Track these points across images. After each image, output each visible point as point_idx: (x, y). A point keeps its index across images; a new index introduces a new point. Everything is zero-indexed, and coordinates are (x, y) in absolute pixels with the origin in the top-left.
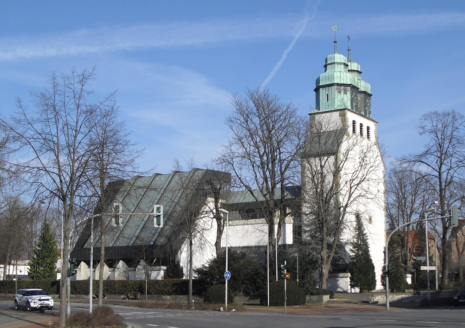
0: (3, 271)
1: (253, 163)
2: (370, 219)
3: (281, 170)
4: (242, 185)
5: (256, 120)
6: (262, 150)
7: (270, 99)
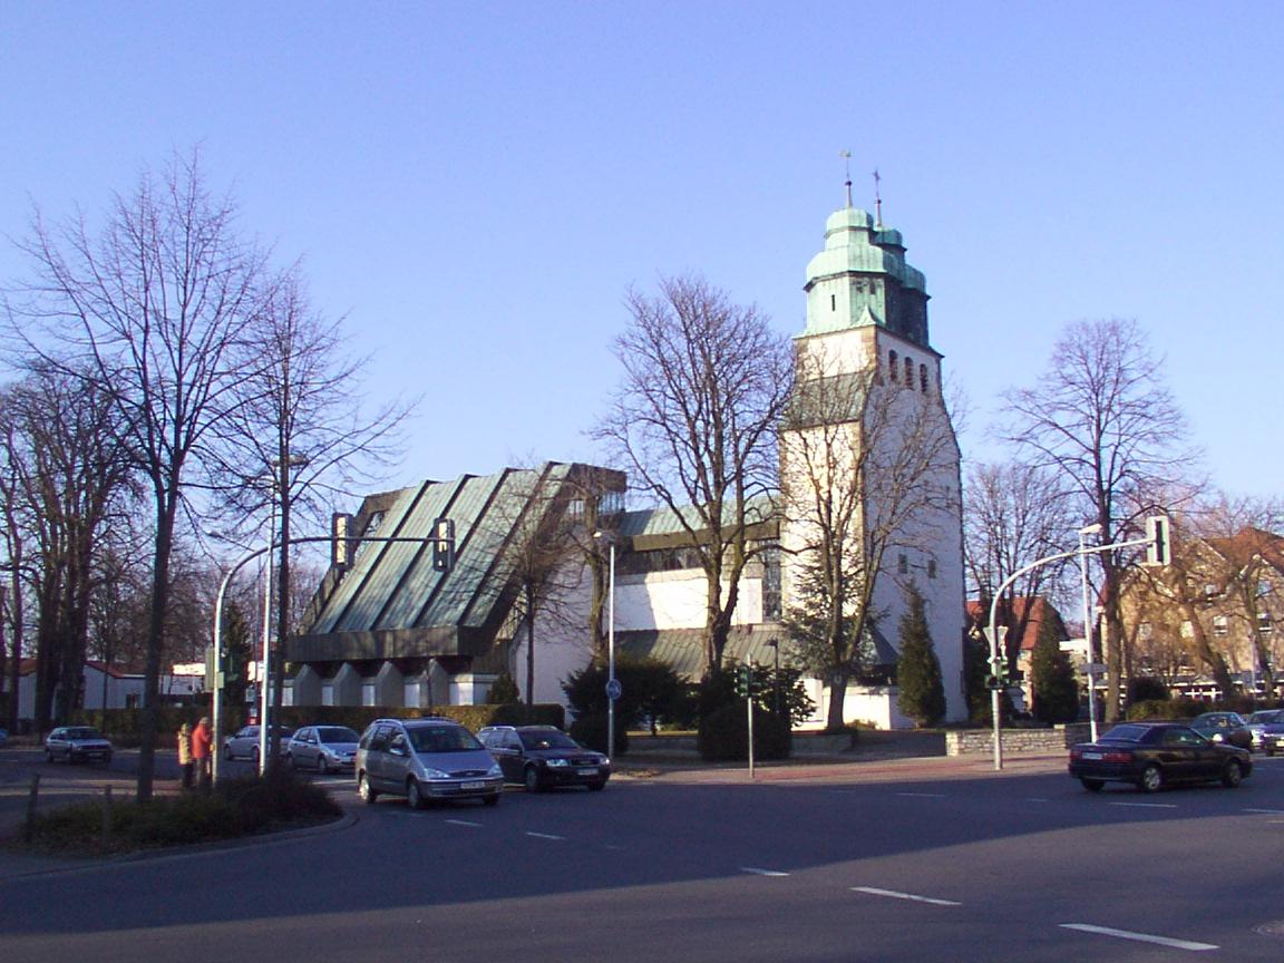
0: (968, 595)
1: (672, 436)
2: (932, 567)
3: (736, 452)
4: (650, 485)
5: (680, 343)
6: (693, 408)
7: (709, 293)
